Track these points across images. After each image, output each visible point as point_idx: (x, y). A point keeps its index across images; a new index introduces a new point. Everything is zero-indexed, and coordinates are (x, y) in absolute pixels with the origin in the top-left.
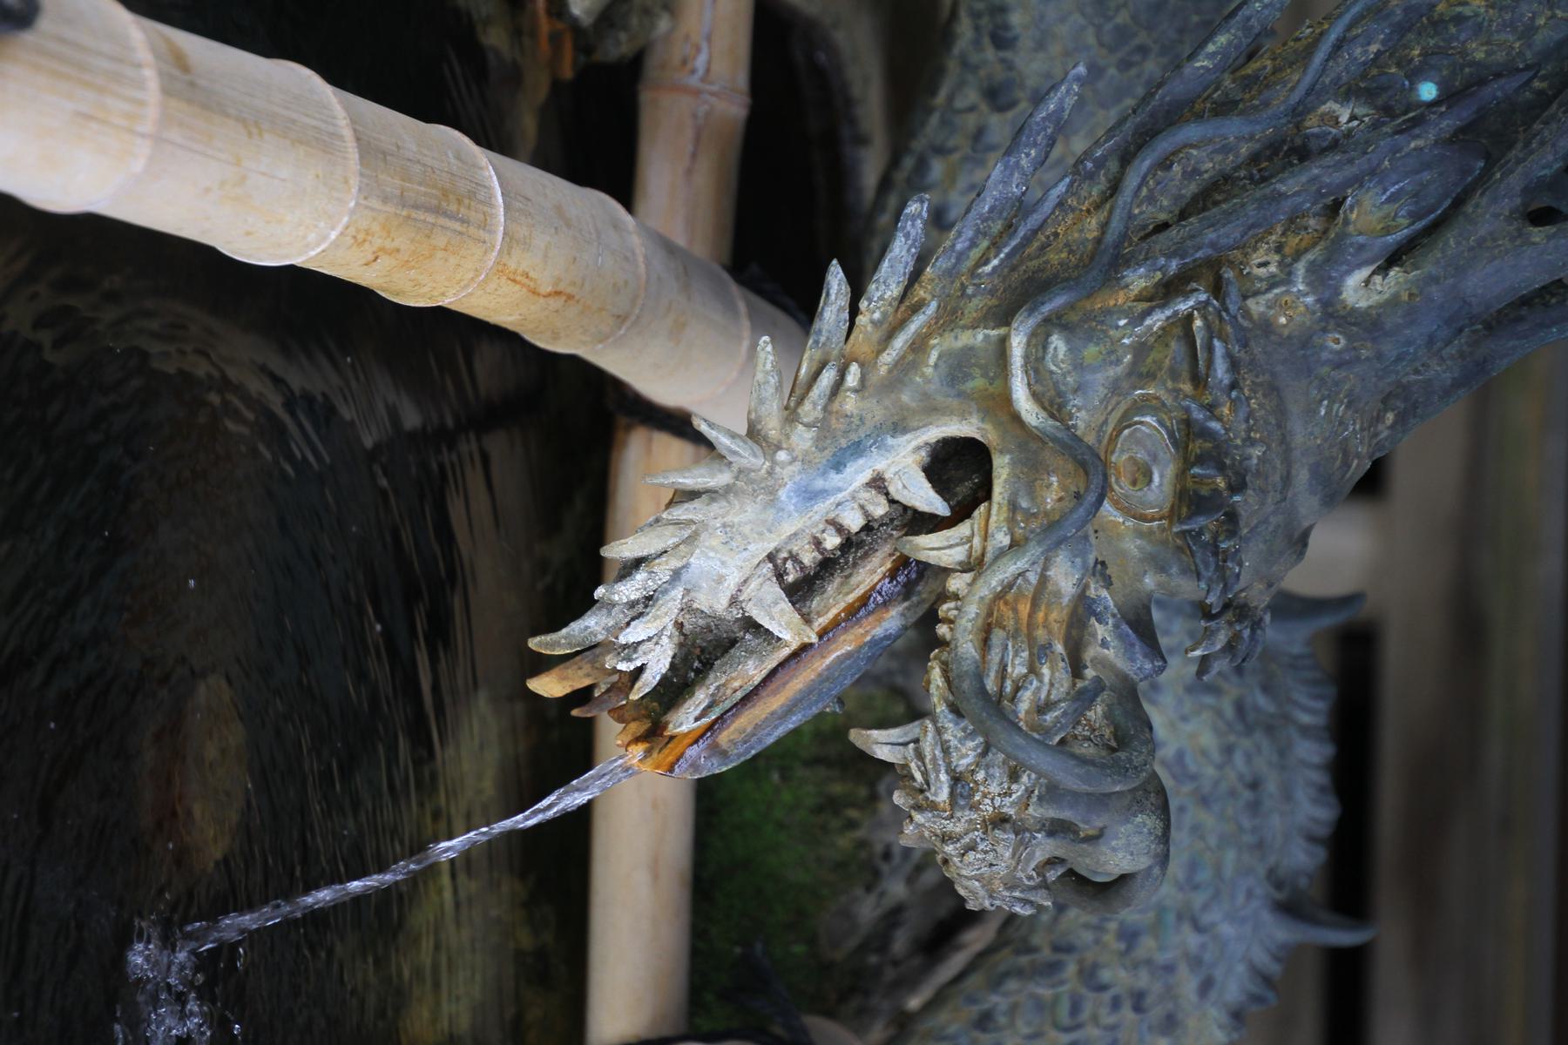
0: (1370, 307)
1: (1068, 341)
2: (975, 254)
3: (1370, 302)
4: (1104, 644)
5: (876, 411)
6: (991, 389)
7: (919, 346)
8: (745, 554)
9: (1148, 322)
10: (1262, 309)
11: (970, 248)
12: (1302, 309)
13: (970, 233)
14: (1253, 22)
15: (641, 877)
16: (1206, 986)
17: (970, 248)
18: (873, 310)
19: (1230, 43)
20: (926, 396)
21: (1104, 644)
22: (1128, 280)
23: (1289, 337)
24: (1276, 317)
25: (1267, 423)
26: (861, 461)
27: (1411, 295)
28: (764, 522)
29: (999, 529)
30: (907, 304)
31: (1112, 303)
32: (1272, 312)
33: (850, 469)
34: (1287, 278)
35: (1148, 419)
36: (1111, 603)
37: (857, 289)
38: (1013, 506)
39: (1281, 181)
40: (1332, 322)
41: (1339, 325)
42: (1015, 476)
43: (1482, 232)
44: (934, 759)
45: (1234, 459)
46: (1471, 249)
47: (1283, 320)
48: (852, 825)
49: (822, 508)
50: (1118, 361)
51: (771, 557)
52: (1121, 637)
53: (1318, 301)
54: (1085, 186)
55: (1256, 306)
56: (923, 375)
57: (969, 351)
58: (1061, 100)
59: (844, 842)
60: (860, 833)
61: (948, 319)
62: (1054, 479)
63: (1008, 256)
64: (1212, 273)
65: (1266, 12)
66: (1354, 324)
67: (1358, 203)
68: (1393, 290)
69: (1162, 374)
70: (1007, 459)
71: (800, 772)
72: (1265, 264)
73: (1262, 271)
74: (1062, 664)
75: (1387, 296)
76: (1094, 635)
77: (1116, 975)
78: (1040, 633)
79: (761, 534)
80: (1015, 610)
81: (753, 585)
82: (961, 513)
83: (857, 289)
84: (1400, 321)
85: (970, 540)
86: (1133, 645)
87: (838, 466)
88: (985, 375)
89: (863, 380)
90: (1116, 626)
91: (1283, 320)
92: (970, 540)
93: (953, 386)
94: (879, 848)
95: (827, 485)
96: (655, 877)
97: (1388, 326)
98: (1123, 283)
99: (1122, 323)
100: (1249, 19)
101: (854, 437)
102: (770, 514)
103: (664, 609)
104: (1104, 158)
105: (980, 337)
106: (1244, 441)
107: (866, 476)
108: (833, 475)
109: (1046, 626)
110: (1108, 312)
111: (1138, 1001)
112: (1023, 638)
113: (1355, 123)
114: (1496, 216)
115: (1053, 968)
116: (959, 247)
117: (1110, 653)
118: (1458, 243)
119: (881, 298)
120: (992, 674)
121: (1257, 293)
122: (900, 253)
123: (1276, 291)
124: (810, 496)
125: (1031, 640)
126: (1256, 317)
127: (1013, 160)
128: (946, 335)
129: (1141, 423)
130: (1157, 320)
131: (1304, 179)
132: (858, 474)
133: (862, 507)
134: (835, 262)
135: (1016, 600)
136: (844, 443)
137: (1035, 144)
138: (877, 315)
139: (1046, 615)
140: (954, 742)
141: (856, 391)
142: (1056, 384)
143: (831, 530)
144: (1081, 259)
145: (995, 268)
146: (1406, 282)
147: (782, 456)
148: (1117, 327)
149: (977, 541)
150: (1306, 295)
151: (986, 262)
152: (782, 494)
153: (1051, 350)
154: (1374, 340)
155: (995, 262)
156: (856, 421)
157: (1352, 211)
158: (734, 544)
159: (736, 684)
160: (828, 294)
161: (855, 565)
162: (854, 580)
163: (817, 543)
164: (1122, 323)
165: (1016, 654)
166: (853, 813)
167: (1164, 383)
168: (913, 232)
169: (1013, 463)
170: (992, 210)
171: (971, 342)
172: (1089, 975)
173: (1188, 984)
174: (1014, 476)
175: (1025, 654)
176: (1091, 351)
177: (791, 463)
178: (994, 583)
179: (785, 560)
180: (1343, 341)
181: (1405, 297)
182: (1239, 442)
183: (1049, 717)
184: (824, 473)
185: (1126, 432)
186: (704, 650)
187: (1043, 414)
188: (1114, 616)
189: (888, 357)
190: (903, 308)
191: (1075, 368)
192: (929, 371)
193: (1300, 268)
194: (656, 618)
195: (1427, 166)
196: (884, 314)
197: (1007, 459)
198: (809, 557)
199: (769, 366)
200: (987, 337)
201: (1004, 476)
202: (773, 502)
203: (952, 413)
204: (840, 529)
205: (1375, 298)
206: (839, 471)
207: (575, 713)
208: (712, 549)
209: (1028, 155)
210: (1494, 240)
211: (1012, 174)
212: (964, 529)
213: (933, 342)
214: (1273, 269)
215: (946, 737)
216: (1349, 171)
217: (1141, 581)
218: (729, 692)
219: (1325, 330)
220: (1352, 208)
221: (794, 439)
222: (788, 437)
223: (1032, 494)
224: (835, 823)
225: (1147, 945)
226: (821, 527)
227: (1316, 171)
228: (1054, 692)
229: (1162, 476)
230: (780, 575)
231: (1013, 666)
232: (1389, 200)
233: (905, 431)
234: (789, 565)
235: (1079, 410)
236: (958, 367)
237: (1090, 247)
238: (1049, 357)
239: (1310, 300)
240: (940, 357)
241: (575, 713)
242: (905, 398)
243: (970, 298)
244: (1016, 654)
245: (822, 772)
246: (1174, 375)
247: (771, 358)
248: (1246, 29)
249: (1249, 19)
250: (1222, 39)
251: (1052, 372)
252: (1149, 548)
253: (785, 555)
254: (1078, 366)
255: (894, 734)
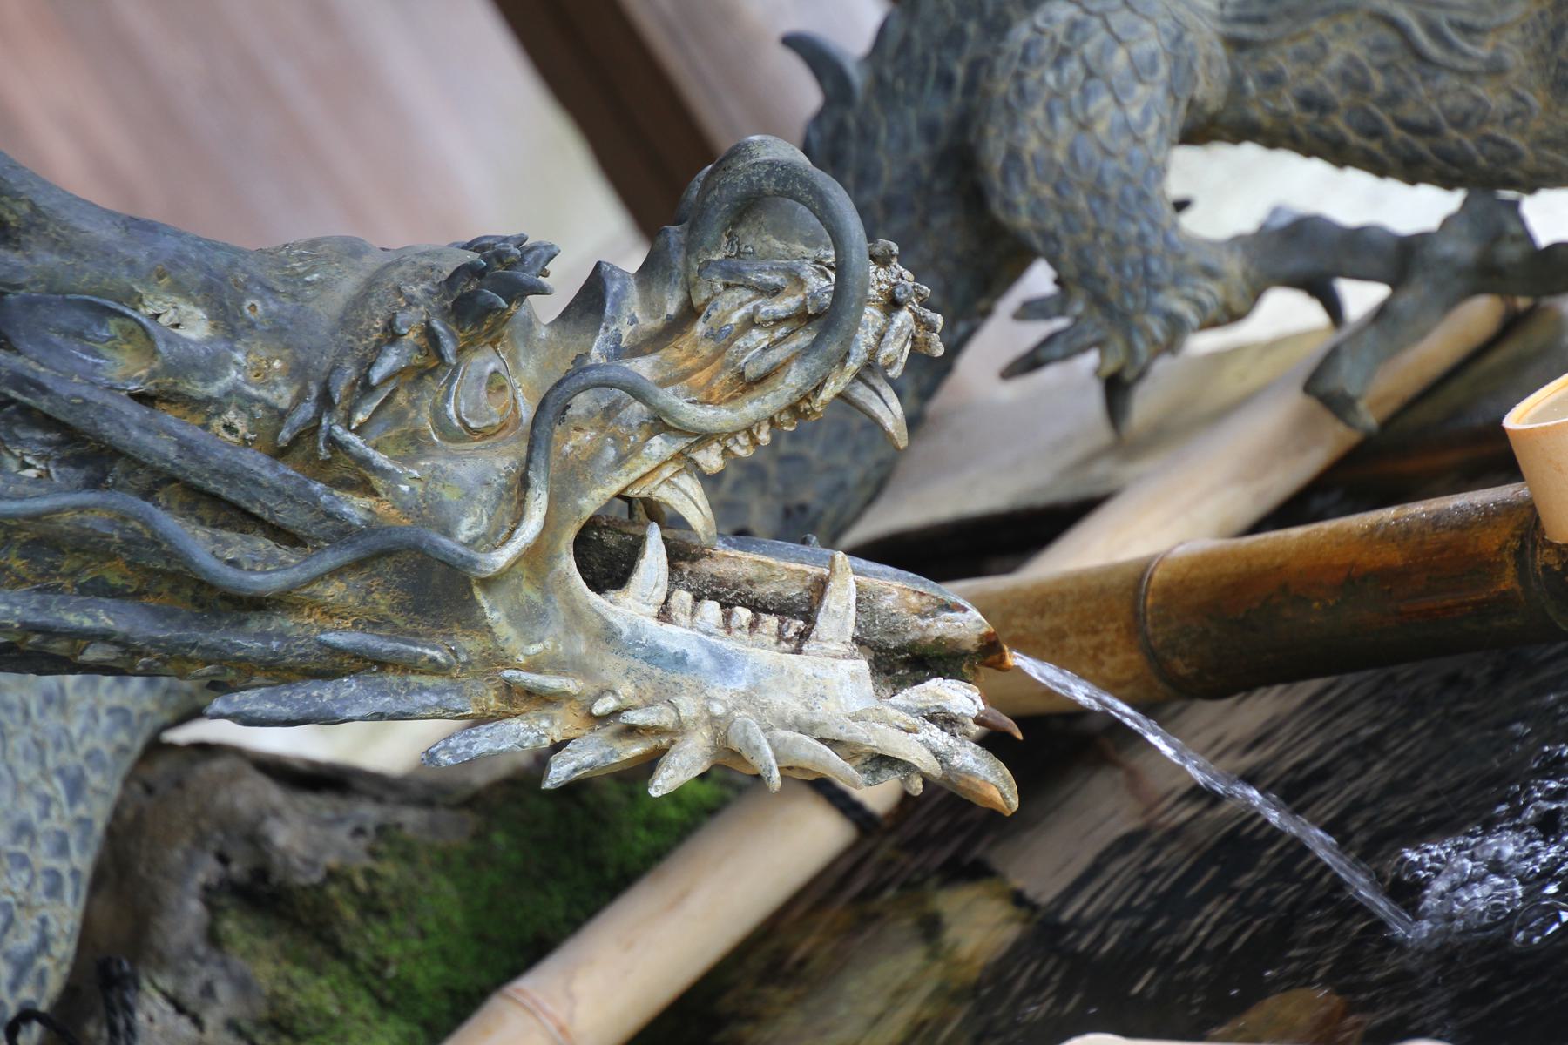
0: (196, 305)
1: (457, 522)
2: (427, 681)
3: (192, 308)
4: (633, 321)
5: (611, 666)
6: (525, 573)
7: (534, 666)
8: (819, 672)
9: (388, 465)
10: (283, 389)
11: (427, 689)
12: (252, 357)
13: (416, 698)
14: (33, 604)
15: (699, 902)
17: (427, 689)
19: (68, 610)
20: (568, 631)
21: (633, 321)
22: (362, 515)
23: (287, 346)
24: (280, 372)
25: (380, 303)
26: (662, 642)
27: (160, 278)
28: (777, 681)
29: (650, 456)
31: (394, 512)
32: (278, 379)
33: (675, 647)
34: (234, 392)
35: (451, 411)
36: (599, 339)
38: (621, 460)
39: (165, 458)
40: (239, 325)
41: (236, 318)
42: (593, 482)
43: (56, 258)
44: (897, 336)
45: (440, 301)
46: (79, 255)
47: (277, 364)
48: (370, 875)
49: (728, 645)
50: (435, 468)
51: (798, 651)
52: (617, 307)
53: (235, 350)
54: (293, 634)
55: (283, 396)
56: (555, 647)
57: (511, 618)
58: (257, 701)
59: (388, 868)
60: (368, 862)
62: (567, 448)
63: (415, 645)
64: (302, 446)
65: (16, 600)
66: (222, 305)
67: (127, 377)
68: (167, 298)
69: (406, 427)
70: (583, 502)
71: (363, 955)
72: (229, 428)
73: (241, 425)
74: (714, 314)
75: (175, 299)
76: (634, 334)
78: (706, 349)
79: (791, 674)
80: (709, 382)
81: (833, 647)
82: (653, 510)
84: (189, 270)
85: (667, 481)
86: (616, 294)
87: (680, 660)
88: (519, 588)
89: (601, 694)
90: (613, 320)
91: (277, 364)
92: (667, 481)
93: (545, 612)
94: (363, 842)
95: (704, 654)
96: (683, 896)
97: (202, 276)
98: (369, 517)
99: (405, 488)
100: (36, 610)
101: (645, 667)
102: (767, 682)
103: (924, 697)
104: (257, 636)
105: (495, 615)
106: (417, 306)
107: (667, 627)
108: (691, 658)
109: (694, 352)
110: (406, 510)
112: (726, 356)
113: (28, 459)
114: (31, 258)
116: (435, 699)
117: (637, 310)
118: (83, 271)
119: (530, 729)
120: (793, 344)
121: (270, 407)
123: (254, 392)
124: (724, 663)
125: (718, 354)
126: (297, 387)
127: (335, 706)
128: (509, 652)
129: (459, 416)
131: (148, 439)
132: (674, 637)
133: (693, 614)
134: (547, 785)
135: (701, 389)
136: (658, 672)
137: (308, 696)
138: (545, 723)
139: (685, 360)
140: (871, 332)
141: (614, 693)
142: (495, 507)
143: (734, 622)
144: (370, 577)
145: (434, 648)
146: (150, 291)
147: (718, 709)
148: (412, 489)
149: (667, 472)
150: (237, 364)
151: (433, 660)
152: (742, 686)
153: (472, 533)
154: (223, 279)
155: (427, 651)
156: (633, 675)
157: (139, 378)
158: (818, 689)
159: (913, 599)
160: (575, 770)
161: (736, 586)
162: (752, 572)
163: (753, 626)
164: (405, 488)
165: (748, 349)
166: (361, 883)
167: (415, 418)
168: (463, 742)
169: (583, 492)
170: (385, 694)
171: (504, 621)
174: (594, 482)
175: (740, 343)
176: (449, 495)
177: (715, 699)
178: (711, 412)
179: (788, 641)
180: (248, 303)
181: (166, 281)
182: (422, 308)
183: (776, 279)
184: (696, 667)
185: (473, 425)
186: (901, 661)
187: (531, 493)
188: (607, 329)
189: (571, 685)
190: (516, 710)
191: (473, 498)
192: (548, 643)
193: (215, 389)
194: (937, 696)
195: (47, 344)
196: (539, 718)
197: (583, 502)
198: (771, 622)
199: (671, 772)
200: (492, 609)
201: (601, 491)
202: (755, 688)
203: (569, 593)
204: (727, 617)
205: (184, 307)
206: (685, 655)
207: (1019, 736)
208: (838, 703)
209: (321, 696)
210: (56, 242)
211: (345, 698)
212: (664, 494)
213: (523, 660)
214: (230, 416)
215: (873, 342)
216: (108, 399)
217: (549, 339)
218: (925, 600)
219: (252, 325)
220: (137, 379)
221: (694, 713)
222: (696, 719)
223: (597, 454)
224: (384, 889)
226: (738, 633)
227: (135, 433)
228: (745, 298)
229: (487, 363)
230: (803, 636)
231: (760, 342)
232: (100, 356)
233: (608, 626)
234: (790, 633)
235: (498, 471)
237: (351, 579)
238: (479, 531)
239: (239, 357)
240: (532, 642)
241: (1019, 736)
242: (582, 648)
243: (468, 653)
244: (748, 349)
245: (347, 941)
246: (400, 416)
247: (664, 775)
248: (45, 606)
249: (36, 610)
250: (73, 619)
251: (489, 518)
252: (522, 350)
253: (784, 644)
254: (469, 496)
255: (877, 407)
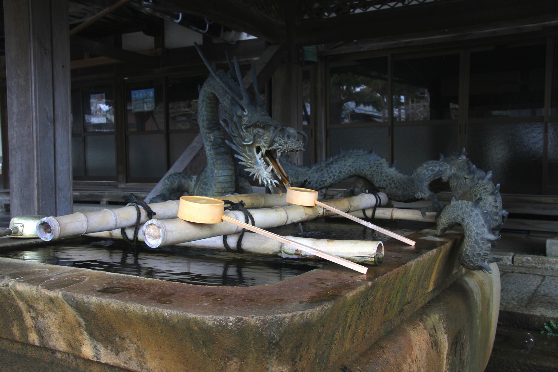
7: (248, 156)
16: (378, 160)
18: (244, 160)
30: (244, 157)
37: (242, 161)
61: (246, 153)
77: (374, 169)
83: (242, 161)
111: (377, 166)
115: (373, 175)
122: (239, 157)
124: (260, 166)
130: (244, 131)
132: (259, 161)
172: (374, 171)
173: (377, 162)
225: (372, 166)
236: (250, 151)
